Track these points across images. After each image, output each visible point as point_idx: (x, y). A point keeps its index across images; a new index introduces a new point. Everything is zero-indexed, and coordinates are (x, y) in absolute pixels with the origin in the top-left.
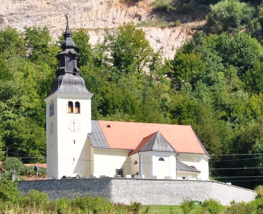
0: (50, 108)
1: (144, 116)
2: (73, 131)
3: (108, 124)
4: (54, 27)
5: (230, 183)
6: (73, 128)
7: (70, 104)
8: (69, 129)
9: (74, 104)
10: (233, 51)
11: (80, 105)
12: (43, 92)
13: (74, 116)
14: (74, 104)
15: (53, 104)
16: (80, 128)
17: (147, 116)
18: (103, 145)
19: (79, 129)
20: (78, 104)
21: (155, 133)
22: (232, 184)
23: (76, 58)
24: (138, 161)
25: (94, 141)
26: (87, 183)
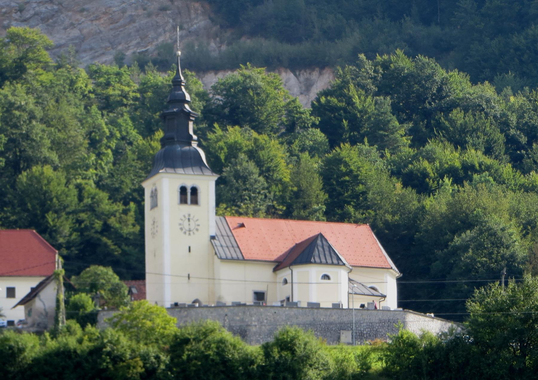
0: (152, 196)
1: (165, 324)
2: (187, 233)
3: (241, 223)
4: (111, 29)
5: (432, 315)
6: (187, 227)
7: (183, 190)
8: (181, 229)
9: (189, 191)
10: (394, 130)
11: (199, 191)
12: (68, 151)
13: (189, 208)
14: (189, 191)
15: (156, 190)
16: (198, 227)
17: (446, 84)
18: (235, 256)
19: (197, 230)
20: (194, 191)
21: (339, 259)
22: (435, 316)
23: (191, 118)
24: (289, 280)
25: (220, 249)
26: (212, 313)
